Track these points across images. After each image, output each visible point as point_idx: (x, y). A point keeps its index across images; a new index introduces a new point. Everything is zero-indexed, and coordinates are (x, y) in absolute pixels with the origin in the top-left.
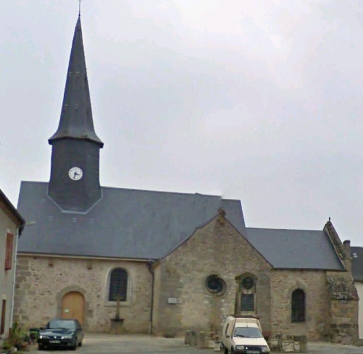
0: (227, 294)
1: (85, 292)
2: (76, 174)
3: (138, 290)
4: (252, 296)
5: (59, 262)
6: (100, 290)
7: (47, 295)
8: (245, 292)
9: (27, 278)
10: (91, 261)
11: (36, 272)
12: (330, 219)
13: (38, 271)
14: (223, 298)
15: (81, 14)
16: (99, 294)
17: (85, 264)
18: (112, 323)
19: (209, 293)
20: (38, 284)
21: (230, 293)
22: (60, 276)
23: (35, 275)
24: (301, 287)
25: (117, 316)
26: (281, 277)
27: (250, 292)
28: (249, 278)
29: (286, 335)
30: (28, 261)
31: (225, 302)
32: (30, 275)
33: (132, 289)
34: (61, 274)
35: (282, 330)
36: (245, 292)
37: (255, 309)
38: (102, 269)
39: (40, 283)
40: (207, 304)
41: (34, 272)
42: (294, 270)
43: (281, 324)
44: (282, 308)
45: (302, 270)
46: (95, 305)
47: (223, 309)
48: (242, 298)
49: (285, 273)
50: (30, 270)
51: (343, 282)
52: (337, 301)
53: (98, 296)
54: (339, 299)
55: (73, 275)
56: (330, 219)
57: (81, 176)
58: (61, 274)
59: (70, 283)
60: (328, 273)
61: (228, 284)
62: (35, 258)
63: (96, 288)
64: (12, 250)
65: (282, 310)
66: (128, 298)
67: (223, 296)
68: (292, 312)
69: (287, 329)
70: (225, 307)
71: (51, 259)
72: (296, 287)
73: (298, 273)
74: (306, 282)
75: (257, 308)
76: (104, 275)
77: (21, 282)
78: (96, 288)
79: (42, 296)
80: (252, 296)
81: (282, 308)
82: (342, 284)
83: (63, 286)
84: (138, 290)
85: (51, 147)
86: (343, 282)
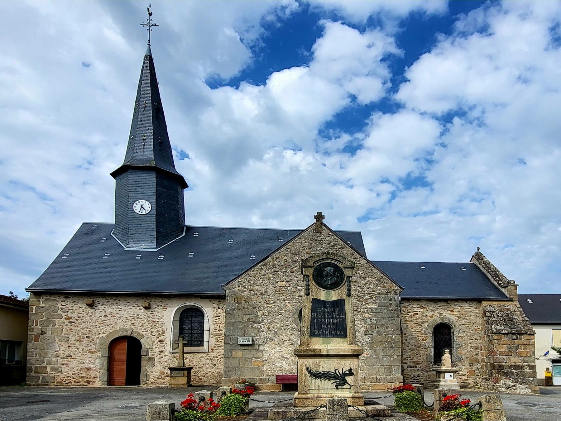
3: (217, 332)
4: (339, 305)
5: (102, 301)
8: (323, 295)
16: (161, 338)
24: (446, 321)
27: (334, 296)
28: (330, 265)
29: (313, 287)
35: (421, 374)
36: (323, 295)
38: (165, 308)
41: (66, 314)
42: (435, 300)
43: (417, 366)
46: (157, 350)
48: (314, 310)
49: (424, 304)
50: (59, 312)
53: (160, 341)
54: (507, 334)
55: (124, 317)
56: (478, 249)
57: (147, 212)
58: (106, 316)
66: (205, 343)
71: (92, 297)
72: (439, 321)
74: (454, 315)
76: (167, 315)
78: (157, 331)
79: (77, 343)
80: (339, 305)
83: (109, 330)
84: (217, 332)
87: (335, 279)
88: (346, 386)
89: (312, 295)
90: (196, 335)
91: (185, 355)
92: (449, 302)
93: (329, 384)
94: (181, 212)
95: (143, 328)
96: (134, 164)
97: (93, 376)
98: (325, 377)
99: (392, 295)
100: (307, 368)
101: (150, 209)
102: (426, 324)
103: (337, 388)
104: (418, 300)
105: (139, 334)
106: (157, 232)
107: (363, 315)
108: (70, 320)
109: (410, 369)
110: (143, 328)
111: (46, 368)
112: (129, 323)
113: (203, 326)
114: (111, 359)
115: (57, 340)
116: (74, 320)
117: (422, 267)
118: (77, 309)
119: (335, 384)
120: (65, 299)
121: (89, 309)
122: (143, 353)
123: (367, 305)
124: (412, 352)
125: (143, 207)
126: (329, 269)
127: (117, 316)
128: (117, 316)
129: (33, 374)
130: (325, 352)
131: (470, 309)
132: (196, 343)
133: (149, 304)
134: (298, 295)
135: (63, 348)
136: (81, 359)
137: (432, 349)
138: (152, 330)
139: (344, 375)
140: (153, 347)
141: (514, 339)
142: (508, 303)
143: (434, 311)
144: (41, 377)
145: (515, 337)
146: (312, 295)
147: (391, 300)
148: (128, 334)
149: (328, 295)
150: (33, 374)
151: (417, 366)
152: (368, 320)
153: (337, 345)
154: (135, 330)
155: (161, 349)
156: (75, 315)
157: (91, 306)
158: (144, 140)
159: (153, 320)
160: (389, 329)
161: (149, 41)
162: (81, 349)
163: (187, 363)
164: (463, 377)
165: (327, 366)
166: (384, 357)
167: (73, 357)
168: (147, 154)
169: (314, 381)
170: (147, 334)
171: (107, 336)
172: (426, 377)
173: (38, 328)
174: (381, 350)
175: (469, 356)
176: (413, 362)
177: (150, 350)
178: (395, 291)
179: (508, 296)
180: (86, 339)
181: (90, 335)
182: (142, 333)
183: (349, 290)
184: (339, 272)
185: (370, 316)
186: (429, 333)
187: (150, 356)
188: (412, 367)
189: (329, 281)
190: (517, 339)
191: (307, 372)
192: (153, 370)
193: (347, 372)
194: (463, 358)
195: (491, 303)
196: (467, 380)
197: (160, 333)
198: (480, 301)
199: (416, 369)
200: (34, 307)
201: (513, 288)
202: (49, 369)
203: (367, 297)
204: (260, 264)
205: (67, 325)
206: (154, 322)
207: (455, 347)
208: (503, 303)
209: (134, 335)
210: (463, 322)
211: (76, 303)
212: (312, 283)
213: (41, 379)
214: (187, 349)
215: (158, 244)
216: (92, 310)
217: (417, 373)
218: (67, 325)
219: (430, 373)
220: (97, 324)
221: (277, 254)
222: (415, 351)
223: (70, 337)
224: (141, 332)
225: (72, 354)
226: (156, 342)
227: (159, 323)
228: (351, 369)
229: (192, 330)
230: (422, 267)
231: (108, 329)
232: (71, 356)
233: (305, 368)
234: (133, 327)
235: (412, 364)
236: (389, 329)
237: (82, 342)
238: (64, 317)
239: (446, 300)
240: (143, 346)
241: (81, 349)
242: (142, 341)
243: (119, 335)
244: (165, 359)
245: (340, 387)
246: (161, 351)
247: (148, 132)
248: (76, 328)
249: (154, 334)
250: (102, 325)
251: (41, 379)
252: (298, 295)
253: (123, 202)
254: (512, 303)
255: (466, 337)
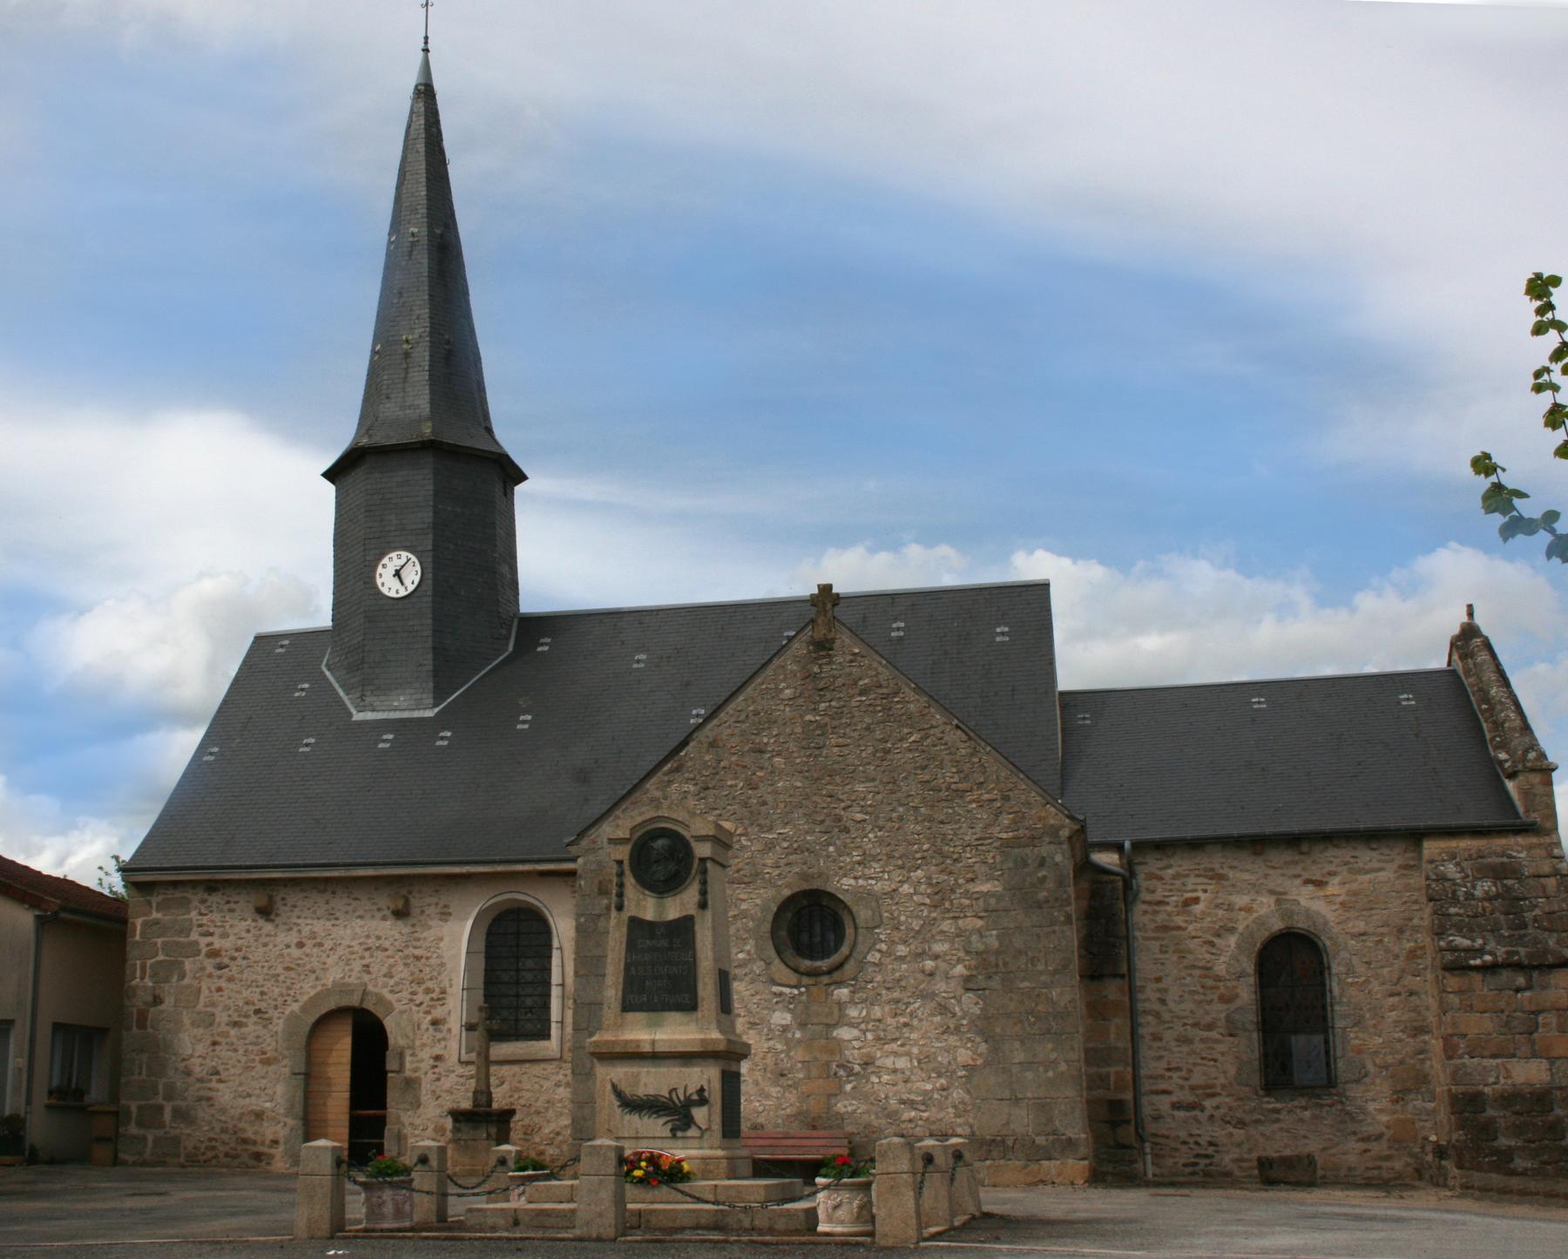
0: (862, 965)
1: (389, 1008)
2: (397, 574)
4: (683, 929)
5: (294, 897)
6: (441, 999)
7: (252, 1028)
9: (188, 965)
10: (402, 888)
11: (218, 943)
12: (1470, 614)
13: (224, 935)
14: (840, 984)
15: (430, 46)
16: (438, 1013)
17: (384, 901)
18: (456, 1130)
19: (793, 978)
20: (224, 985)
21: (874, 957)
22: (295, 952)
23: (213, 954)
24: (1301, 924)
25: (483, 1094)
26: (1197, 886)
27: (673, 909)
30: (189, 902)
31: (852, 1001)
32: (198, 953)
33: (563, 985)
34: (300, 945)
35: (1218, 1132)
36: (648, 908)
37: (707, 989)
38: (445, 915)
39: (231, 979)
40: (785, 1029)
41: (209, 939)
42: (1257, 844)
43: (1208, 1103)
44: (1210, 1027)
45: (1293, 841)
46: (426, 1054)
47: (844, 1033)
48: (631, 945)
49: (1215, 860)
50: (194, 936)
51: (1509, 882)
52: (1477, 977)
53: (435, 1023)
54: (1485, 969)
55: (341, 949)
56: (1470, 614)
58: (300, 945)
59: (333, 976)
60: (1431, 847)
61: (863, 914)
62: (212, 887)
63: (428, 991)
64: (694, 956)
65: (1214, 1034)
67: (836, 976)
68: (1264, 1043)
69: (1241, 1124)
70: (851, 1025)
71: (267, 891)
72: (1277, 925)
73: (1279, 857)
75: (724, 981)
76: (454, 938)
77: (167, 980)
78: (428, 991)
79: (233, 1032)
80: (683, 929)
81: (1210, 1027)
82: (1508, 889)
83: (309, 989)
85: (330, 489)
86: (1509, 882)
87: (672, 867)
88: (693, 1132)
89: (631, 910)
90: (529, 1002)
91: (493, 1069)
92: (1305, 847)
93: (656, 1126)
94: (505, 569)
95: (392, 982)
96: (381, 438)
97: (269, 1136)
98: (650, 1108)
99: (1045, 849)
100: (614, 1087)
101: (417, 579)
102: (1233, 940)
103: (674, 1136)
104: (1195, 845)
105: (380, 1000)
106: (436, 651)
107: (960, 922)
108: (218, 960)
109: (1181, 1114)
110: (392, 982)
111: (160, 1109)
112: (357, 966)
113: (547, 970)
114: (310, 1078)
115: (186, 1021)
116: (226, 961)
117: (1259, 702)
118: (229, 928)
119: (669, 1126)
120: (206, 896)
121: (261, 922)
122: (391, 1064)
123: (970, 886)
124: (1185, 1049)
125: (398, 575)
126: (660, 843)
127: (328, 944)
128: (328, 944)
129: (133, 1129)
130: (647, 1048)
131: (1380, 871)
132: (529, 1026)
133: (407, 902)
134: (769, 862)
135: (201, 1049)
136: (241, 1084)
137: (1255, 1035)
138: (415, 987)
139: (689, 1104)
140: (418, 1043)
141: (1518, 990)
142: (1520, 839)
143: (1255, 888)
144: (150, 1138)
145: (1521, 981)
146: (631, 910)
147: (1042, 864)
148: (354, 1001)
149: (660, 908)
150: (133, 1129)
151: (1208, 1103)
152: (974, 938)
153: (675, 1031)
154: (370, 988)
155: (437, 1051)
156: (227, 944)
157: (265, 912)
158: (407, 355)
159: (417, 952)
160: (1040, 967)
161: (426, 38)
162: (241, 1052)
163: (500, 1098)
164: (1376, 1148)
165: (653, 1081)
166: (1027, 1065)
167: (224, 1075)
168: (415, 403)
169: (627, 1117)
170: (399, 1001)
171: (304, 1009)
172: (1239, 1145)
173: (145, 987)
174: (1017, 1044)
175: (1390, 1059)
176: (1193, 1088)
177: (408, 1052)
178: (1054, 832)
179: (1521, 810)
180: (254, 1018)
181: (263, 1005)
182: (389, 996)
183: (703, 893)
184: (679, 849)
185: (980, 923)
186: (1241, 975)
187: (408, 1073)
188: (1190, 1107)
189: (660, 872)
190: (1529, 988)
191: (613, 1097)
192: (417, 1121)
193: (695, 1097)
194: (1370, 1067)
195: (1453, 844)
196: (1388, 1158)
197: (434, 995)
198: (1415, 836)
199: (1203, 1117)
200: (139, 922)
201: (1535, 778)
202: (167, 1115)
203: (970, 858)
204: (666, 769)
205: (210, 976)
206: (418, 958)
207: (1339, 1024)
208: (1499, 843)
209: (369, 1005)
210: (1361, 926)
211: (232, 906)
212: (630, 880)
213: (150, 1143)
214: (501, 1050)
215: (439, 694)
216: (268, 927)
217: (1207, 1132)
218: (210, 976)
219: (1252, 1131)
220: (280, 970)
221: (709, 731)
222: (1198, 1046)
223: (217, 1011)
224: (386, 993)
225: (220, 1068)
226: (424, 1027)
227: (433, 961)
228: (702, 1090)
229: (517, 983)
230: (1259, 702)
231: (306, 986)
232: (217, 1073)
233: (609, 1087)
234: (366, 978)
235: (1189, 1097)
236: (1040, 967)
237: (244, 1030)
238: (204, 950)
239: (1293, 841)
240: (391, 1041)
241: (241, 1052)
242: (389, 1023)
243: (331, 1004)
244: (447, 1083)
245: (679, 1134)
246: (438, 1058)
247: (417, 331)
248: (232, 986)
249: (419, 998)
250: (293, 974)
251: (150, 1143)
252: (769, 862)
253: (354, 555)
254: (1534, 840)
255: (1376, 986)
